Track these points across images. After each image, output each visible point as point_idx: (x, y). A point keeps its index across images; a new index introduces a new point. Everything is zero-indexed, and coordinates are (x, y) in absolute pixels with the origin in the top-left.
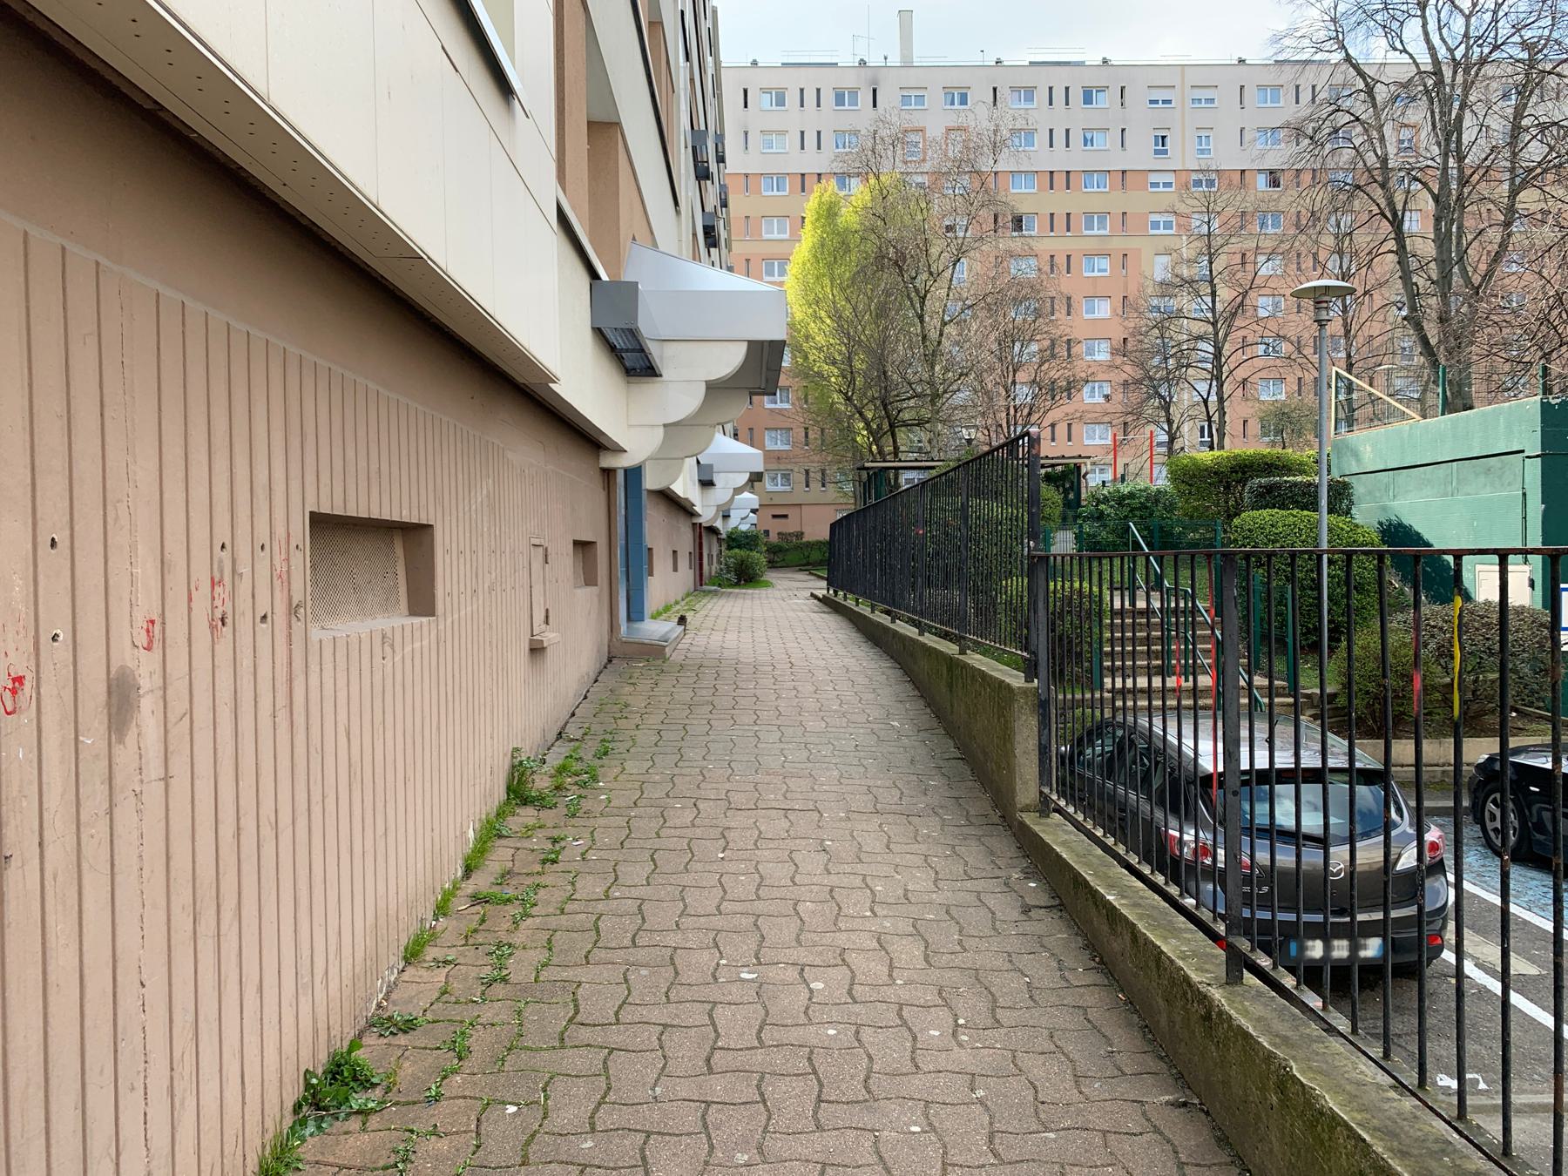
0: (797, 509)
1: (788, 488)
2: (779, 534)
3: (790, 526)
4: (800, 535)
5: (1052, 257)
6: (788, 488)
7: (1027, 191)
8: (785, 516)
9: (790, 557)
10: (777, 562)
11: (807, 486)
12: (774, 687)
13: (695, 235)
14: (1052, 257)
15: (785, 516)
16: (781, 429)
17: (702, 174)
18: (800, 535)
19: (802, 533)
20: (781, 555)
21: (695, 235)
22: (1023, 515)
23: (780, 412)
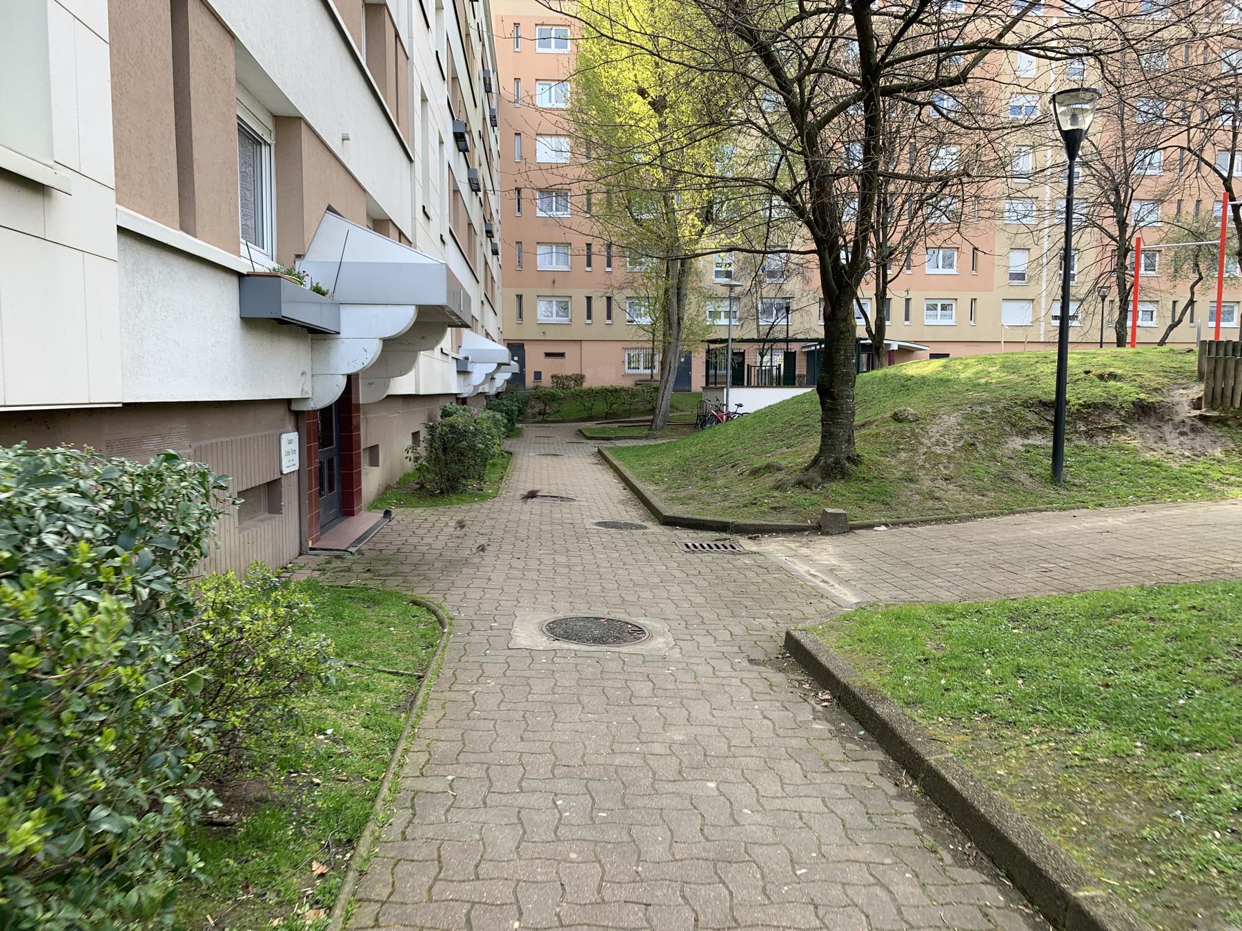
0: (576, 347)
1: (565, 320)
2: (552, 377)
3: (567, 367)
4: (579, 379)
5: (517, 25)
6: (565, 320)
7: (557, 51)
8: (562, 355)
9: (566, 408)
10: (549, 414)
11: (609, 265)
12: (521, 746)
13: (484, 119)
14: (517, 25)
15: (562, 355)
16: (557, 244)
17: (488, 90)
18: (579, 379)
19: (582, 377)
20: (555, 405)
21: (484, 119)
22: (1078, 354)
23: (558, 222)
